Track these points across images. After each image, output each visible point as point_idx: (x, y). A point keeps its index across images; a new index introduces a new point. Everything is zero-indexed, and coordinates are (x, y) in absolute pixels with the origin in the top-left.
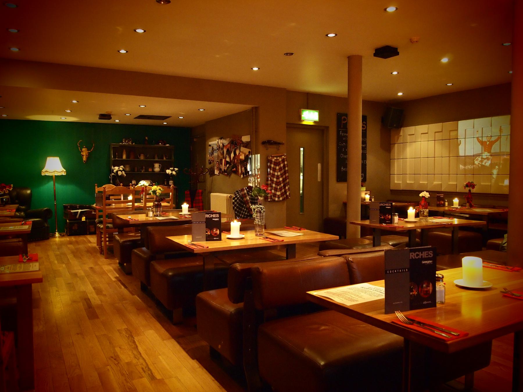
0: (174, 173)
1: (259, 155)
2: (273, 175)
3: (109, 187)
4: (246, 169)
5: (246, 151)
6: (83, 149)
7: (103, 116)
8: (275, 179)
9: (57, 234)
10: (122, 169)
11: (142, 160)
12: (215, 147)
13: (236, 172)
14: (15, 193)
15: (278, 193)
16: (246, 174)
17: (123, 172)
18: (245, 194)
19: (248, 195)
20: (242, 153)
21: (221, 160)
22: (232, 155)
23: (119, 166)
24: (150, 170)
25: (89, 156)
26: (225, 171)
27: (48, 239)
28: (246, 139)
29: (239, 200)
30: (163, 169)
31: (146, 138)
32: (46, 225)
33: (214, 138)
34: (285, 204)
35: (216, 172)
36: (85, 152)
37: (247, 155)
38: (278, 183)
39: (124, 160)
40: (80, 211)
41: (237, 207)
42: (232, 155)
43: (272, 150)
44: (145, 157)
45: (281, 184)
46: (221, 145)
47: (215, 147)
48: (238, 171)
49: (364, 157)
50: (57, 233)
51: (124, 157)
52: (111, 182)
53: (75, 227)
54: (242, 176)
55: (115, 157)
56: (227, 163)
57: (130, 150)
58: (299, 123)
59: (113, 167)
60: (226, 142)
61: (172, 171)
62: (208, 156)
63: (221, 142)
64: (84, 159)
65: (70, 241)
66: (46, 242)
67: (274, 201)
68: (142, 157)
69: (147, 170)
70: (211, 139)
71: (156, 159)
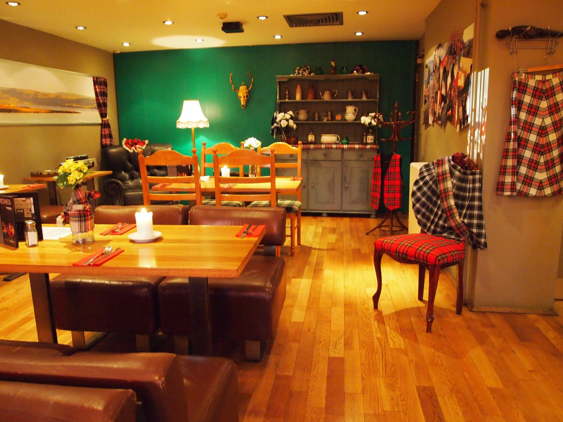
2: (528, 127)
7: (232, 27)
8: (533, 138)
11: (326, 102)
15: (541, 176)
16: (464, 124)
17: (291, 122)
18: (444, 174)
24: (338, 117)
25: (249, 97)
29: (430, 188)
36: (242, 92)
38: (539, 149)
41: (423, 205)
43: (530, 54)
44: (332, 95)
45: (550, 150)
48: (454, 117)
49: (262, 211)
51: (298, 97)
64: (243, 103)
67: (523, 195)
68: (326, 97)
69: (333, 118)
71: (350, 99)
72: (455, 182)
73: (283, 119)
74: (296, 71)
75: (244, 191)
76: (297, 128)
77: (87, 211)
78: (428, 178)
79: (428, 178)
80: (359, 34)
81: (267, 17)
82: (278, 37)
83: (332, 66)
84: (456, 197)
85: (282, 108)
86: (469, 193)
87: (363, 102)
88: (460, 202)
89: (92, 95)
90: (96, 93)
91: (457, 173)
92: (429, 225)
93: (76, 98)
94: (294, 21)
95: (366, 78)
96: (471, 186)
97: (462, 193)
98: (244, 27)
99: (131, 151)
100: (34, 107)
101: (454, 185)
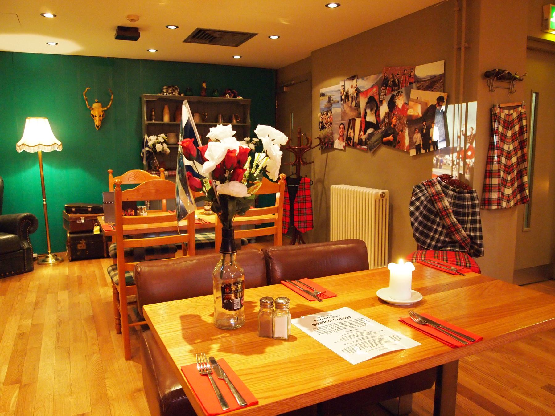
1: (473, 106)
4: (427, 137)
5: (431, 97)
6: (95, 105)
7: (127, 33)
9: (51, 260)
10: (162, 140)
12: (336, 97)
13: (395, 144)
17: (165, 145)
18: (438, 194)
19: (446, 195)
20: (415, 104)
22: (384, 109)
23: (157, 134)
25: (104, 120)
26: (360, 142)
27: (31, 270)
28: (423, 71)
29: (425, 207)
31: (204, 85)
32: (26, 245)
33: (334, 80)
34: (516, 212)
35: (338, 144)
36: (97, 110)
41: (421, 223)
42: (384, 109)
43: (500, 91)
46: (352, 92)
47: (336, 97)
50: (50, 256)
51: (166, 119)
52: (144, 162)
53: (82, 246)
54: (413, 152)
55: (150, 119)
56: (368, 125)
58: (540, 37)
59: (146, 137)
60: (364, 84)
61: (248, 142)
62: (318, 116)
63: (350, 86)
64: (97, 122)
65: (68, 278)
66: (29, 276)
70: (326, 83)
72: (450, 200)
74: (165, 91)
76: (170, 153)
79: (423, 198)
80: (237, 57)
81: (177, 27)
82: (152, 51)
84: (456, 214)
85: (154, 130)
86: (468, 209)
88: (461, 218)
91: (451, 193)
92: (428, 241)
94: (201, 36)
95: (238, 103)
96: (470, 203)
97: (461, 210)
98: (142, 34)
101: (450, 203)
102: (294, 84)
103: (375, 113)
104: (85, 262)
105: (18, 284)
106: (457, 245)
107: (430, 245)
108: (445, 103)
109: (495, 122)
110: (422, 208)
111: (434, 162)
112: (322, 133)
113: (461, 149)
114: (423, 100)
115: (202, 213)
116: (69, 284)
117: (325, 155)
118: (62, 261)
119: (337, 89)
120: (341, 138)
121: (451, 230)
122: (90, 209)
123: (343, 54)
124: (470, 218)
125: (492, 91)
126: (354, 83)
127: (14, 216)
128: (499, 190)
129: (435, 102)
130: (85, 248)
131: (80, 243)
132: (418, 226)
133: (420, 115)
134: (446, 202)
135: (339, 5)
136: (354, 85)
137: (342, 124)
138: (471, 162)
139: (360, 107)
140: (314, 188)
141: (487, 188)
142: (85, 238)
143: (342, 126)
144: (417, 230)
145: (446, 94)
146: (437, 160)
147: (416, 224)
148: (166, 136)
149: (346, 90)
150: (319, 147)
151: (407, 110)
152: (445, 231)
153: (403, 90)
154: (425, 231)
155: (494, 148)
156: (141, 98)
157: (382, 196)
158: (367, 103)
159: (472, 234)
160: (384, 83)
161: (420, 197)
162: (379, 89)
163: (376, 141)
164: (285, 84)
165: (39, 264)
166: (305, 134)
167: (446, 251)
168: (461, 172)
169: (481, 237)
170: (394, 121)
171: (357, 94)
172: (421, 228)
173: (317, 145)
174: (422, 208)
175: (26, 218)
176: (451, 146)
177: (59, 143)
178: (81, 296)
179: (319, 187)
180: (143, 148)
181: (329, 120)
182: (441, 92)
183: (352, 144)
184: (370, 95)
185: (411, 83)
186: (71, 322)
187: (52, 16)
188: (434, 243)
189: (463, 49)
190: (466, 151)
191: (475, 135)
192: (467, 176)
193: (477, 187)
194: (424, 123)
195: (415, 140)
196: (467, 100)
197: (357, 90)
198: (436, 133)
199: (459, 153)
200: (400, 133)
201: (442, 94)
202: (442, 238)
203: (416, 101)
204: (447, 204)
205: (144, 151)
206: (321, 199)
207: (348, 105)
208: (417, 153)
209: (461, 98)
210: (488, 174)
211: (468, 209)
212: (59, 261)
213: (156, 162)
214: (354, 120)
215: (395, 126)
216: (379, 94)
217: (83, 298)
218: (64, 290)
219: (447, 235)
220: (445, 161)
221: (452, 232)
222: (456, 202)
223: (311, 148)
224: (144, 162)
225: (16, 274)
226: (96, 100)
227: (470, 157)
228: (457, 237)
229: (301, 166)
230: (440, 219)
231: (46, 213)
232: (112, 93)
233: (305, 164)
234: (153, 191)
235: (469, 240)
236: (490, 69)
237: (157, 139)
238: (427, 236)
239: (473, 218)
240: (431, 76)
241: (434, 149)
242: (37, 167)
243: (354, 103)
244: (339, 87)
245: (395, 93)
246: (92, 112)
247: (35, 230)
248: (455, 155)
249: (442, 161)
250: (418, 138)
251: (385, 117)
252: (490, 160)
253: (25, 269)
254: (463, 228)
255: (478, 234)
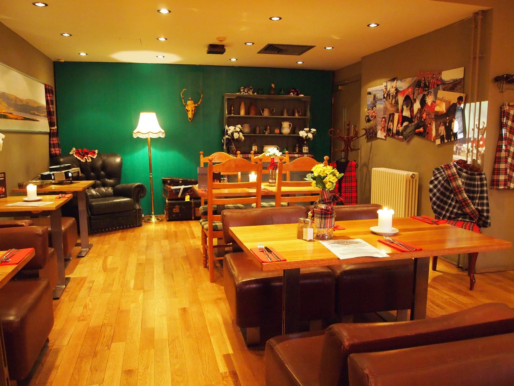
0: (310, 135)
1: (485, 104)
3: (219, 158)
5: (453, 97)
6: (189, 102)
7: (216, 49)
10: (239, 130)
11: (266, 118)
12: (380, 95)
13: (425, 135)
14: (100, 163)
17: (241, 134)
18: (453, 175)
19: (460, 176)
21: (392, 115)
22: (417, 106)
23: (235, 125)
24: (277, 131)
25: (196, 113)
27: (141, 225)
28: (448, 76)
29: (442, 185)
30: (294, 130)
31: (273, 85)
32: (138, 207)
33: (378, 81)
35: (381, 134)
36: (190, 106)
37: (455, 105)
39: (242, 117)
40: (182, 187)
41: (438, 198)
42: (417, 106)
44: (271, 112)
46: (393, 91)
47: (380, 95)
50: (153, 216)
51: (242, 113)
52: (225, 147)
53: (176, 210)
54: (438, 142)
55: (230, 112)
56: (404, 119)
57: (251, 104)
59: (226, 127)
60: (402, 85)
61: (307, 132)
62: (365, 111)
63: (391, 86)
64: (190, 115)
65: (167, 232)
66: (138, 231)
68: (266, 113)
69: (272, 132)
71: (286, 116)
72: (463, 180)
73: (234, 130)
74: (242, 90)
75: (237, 195)
77: (328, 211)
78: (440, 178)
79: (440, 178)
81: (253, 44)
82: (233, 60)
83: (272, 88)
84: (467, 191)
85: (232, 122)
86: (478, 188)
87: (295, 118)
88: (471, 195)
89: (44, 103)
90: (47, 101)
91: (464, 174)
93: (36, 106)
94: (271, 49)
95: (300, 100)
96: (479, 183)
97: (472, 189)
99: (83, 161)
100: (16, 113)
101: (463, 183)
102: (347, 83)
103: (410, 109)
104: (179, 222)
105: (133, 234)
106: (468, 216)
107: (445, 215)
108: (463, 102)
109: (504, 118)
110: (439, 186)
111: (455, 150)
112: (368, 125)
113: (474, 139)
114: (447, 99)
115: (267, 185)
116: (167, 236)
117: (370, 143)
118: (162, 221)
119: (381, 89)
120: (383, 130)
121: (463, 204)
122: (180, 182)
123: (387, 59)
124: (478, 195)
125: (502, 92)
126: (394, 84)
127: (130, 185)
128: (506, 173)
129: (456, 101)
130: (178, 212)
131: (175, 208)
132: (436, 201)
133: (445, 111)
134: (460, 182)
135: (378, 25)
136: (394, 86)
137: (384, 118)
138: (482, 150)
139: (398, 104)
140: (360, 170)
141: (496, 171)
142: (179, 204)
143: (383, 119)
144: (434, 203)
145: (465, 95)
146: (457, 148)
147: (434, 199)
148: (242, 126)
149: (388, 90)
150: (365, 136)
151: (435, 107)
152: (458, 205)
153: (432, 91)
154: (442, 205)
155: (502, 139)
156: (223, 97)
157: (412, 177)
158: (404, 101)
159: (479, 208)
160: (418, 85)
161: (438, 178)
162: (414, 89)
163: (410, 132)
164: (340, 84)
165: (145, 222)
166: (355, 126)
167: (458, 220)
168: (475, 158)
169: (488, 211)
170: (424, 116)
171: (396, 93)
172: (438, 202)
173: (364, 135)
174: (439, 186)
175: (138, 186)
176: (467, 137)
177: (163, 131)
178: (177, 243)
179: (365, 169)
180: (224, 136)
181: (373, 114)
182: (461, 92)
183: (391, 135)
184: (407, 93)
185: (438, 85)
186: (172, 259)
187: (164, 40)
188: (448, 214)
189: (477, 59)
190: (479, 141)
191: (486, 128)
192: (479, 162)
193: (487, 172)
194: (448, 118)
195: (440, 132)
196: (480, 99)
197: (397, 89)
198: (456, 126)
199: (473, 142)
200: (429, 125)
201: (462, 95)
202: (455, 210)
203: (442, 100)
204: (460, 183)
205: (224, 138)
206: (365, 182)
207: (389, 102)
208: (441, 142)
209: (475, 98)
210: (497, 160)
211: (478, 188)
212: (160, 221)
213: (233, 147)
214: (393, 114)
215: (425, 120)
216: (414, 94)
217: (179, 245)
218: (164, 239)
219: (459, 209)
220: (462, 149)
221: (463, 206)
222: (468, 182)
223: (358, 138)
224: (225, 147)
225: (130, 227)
226: (190, 99)
227: (482, 146)
228: (468, 210)
229: (349, 152)
230: (454, 195)
231: (151, 185)
232: (202, 93)
233: (352, 150)
234: (234, 166)
235: (477, 213)
236: (500, 74)
237: (235, 129)
238: (443, 209)
239: (481, 195)
240: (453, 80)
241: (454, 139)
242: (147, 148)
243: (394, 101)
244: (382, 87)
245: (426, 93)
246: (186, 108)
247: (144, 196)
248: (470, 144)
249: (460, 149)
250: (442, 129)
251: (418, 112)
252: (499, 149)
253: (136, 224)
254: (473, 203)
255: (485, 208)
